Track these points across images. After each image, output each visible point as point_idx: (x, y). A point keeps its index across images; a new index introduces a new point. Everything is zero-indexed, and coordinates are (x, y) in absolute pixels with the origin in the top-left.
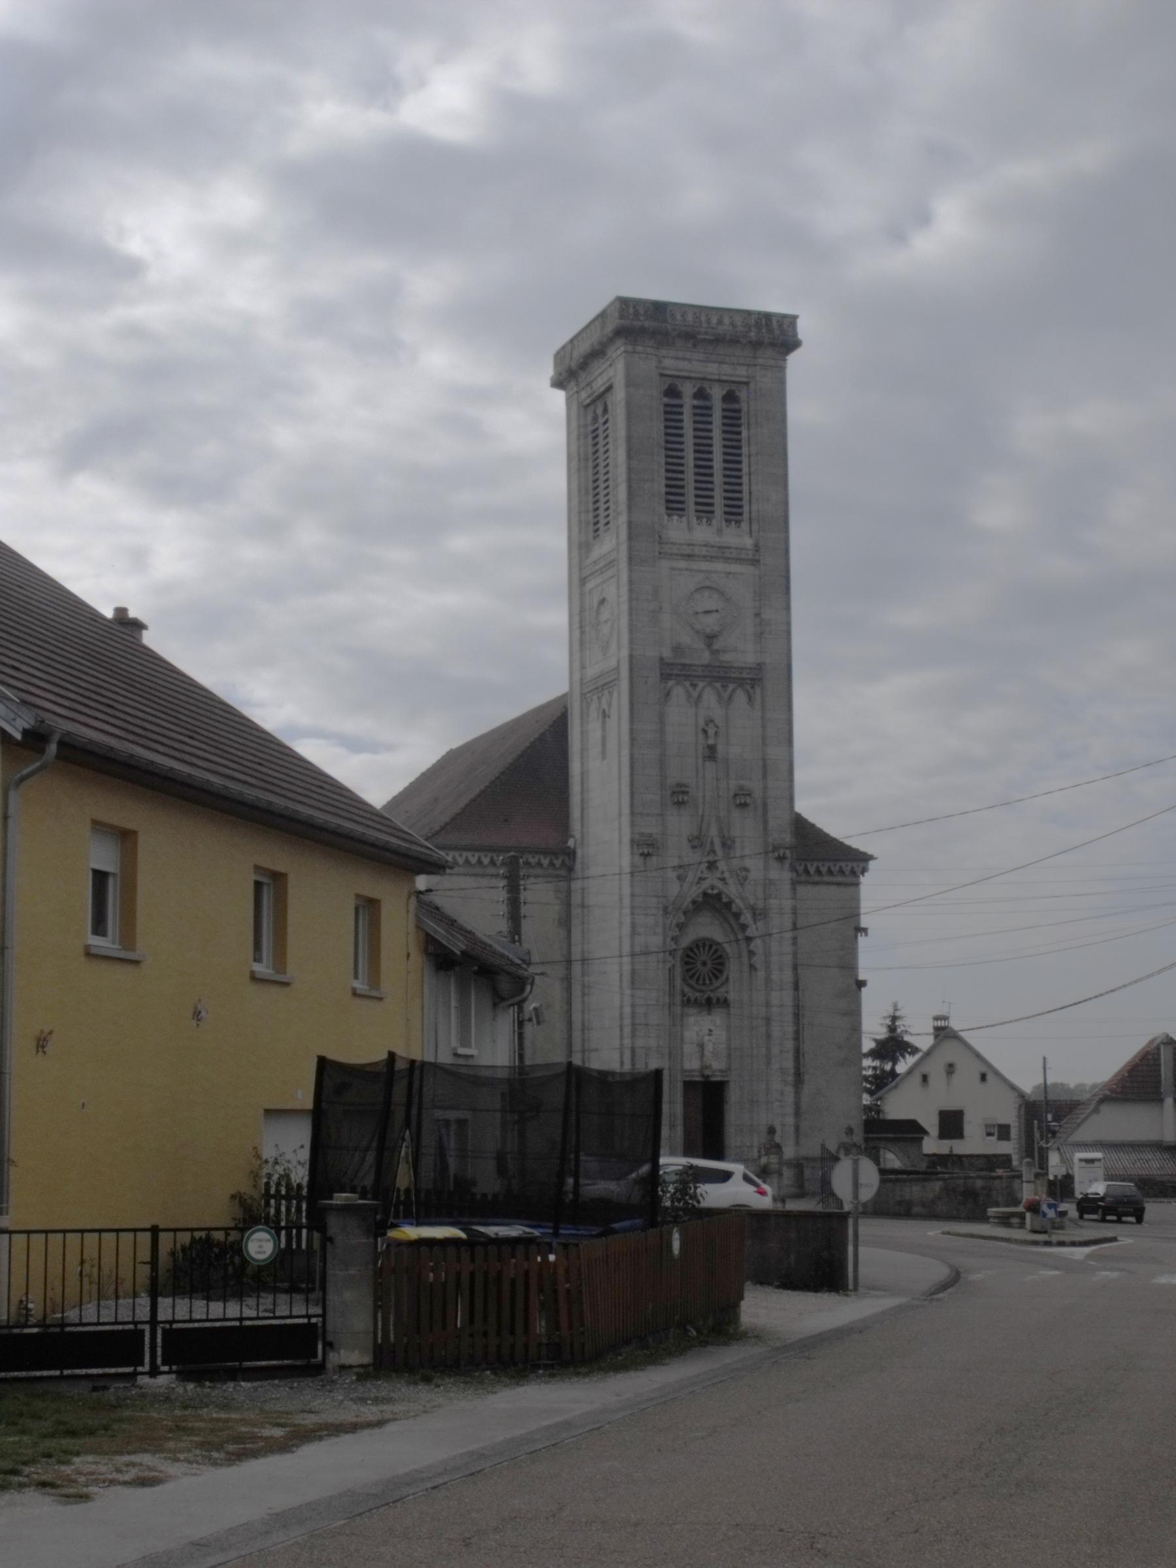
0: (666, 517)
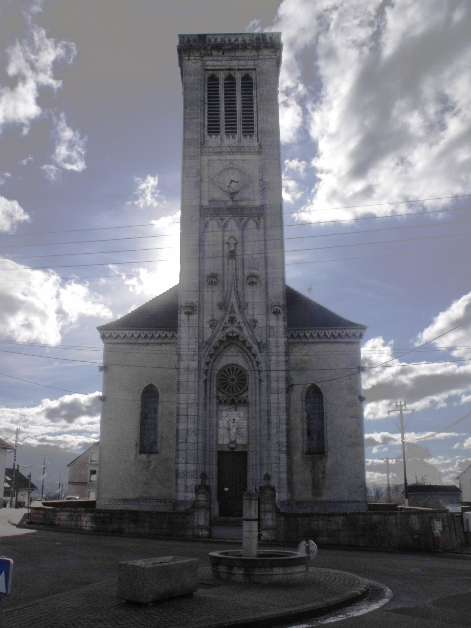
0: (208, 137)
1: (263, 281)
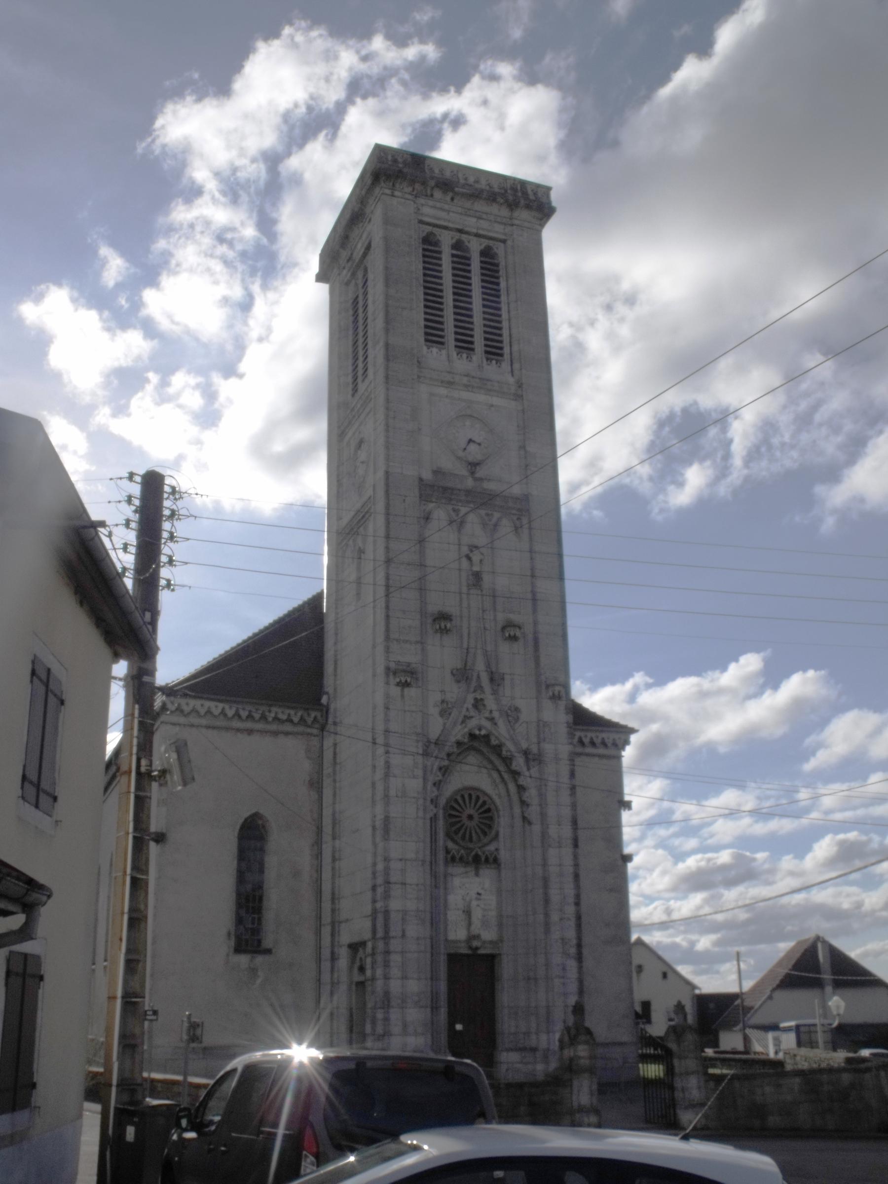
0: (425, 348)
1: (530, 637)
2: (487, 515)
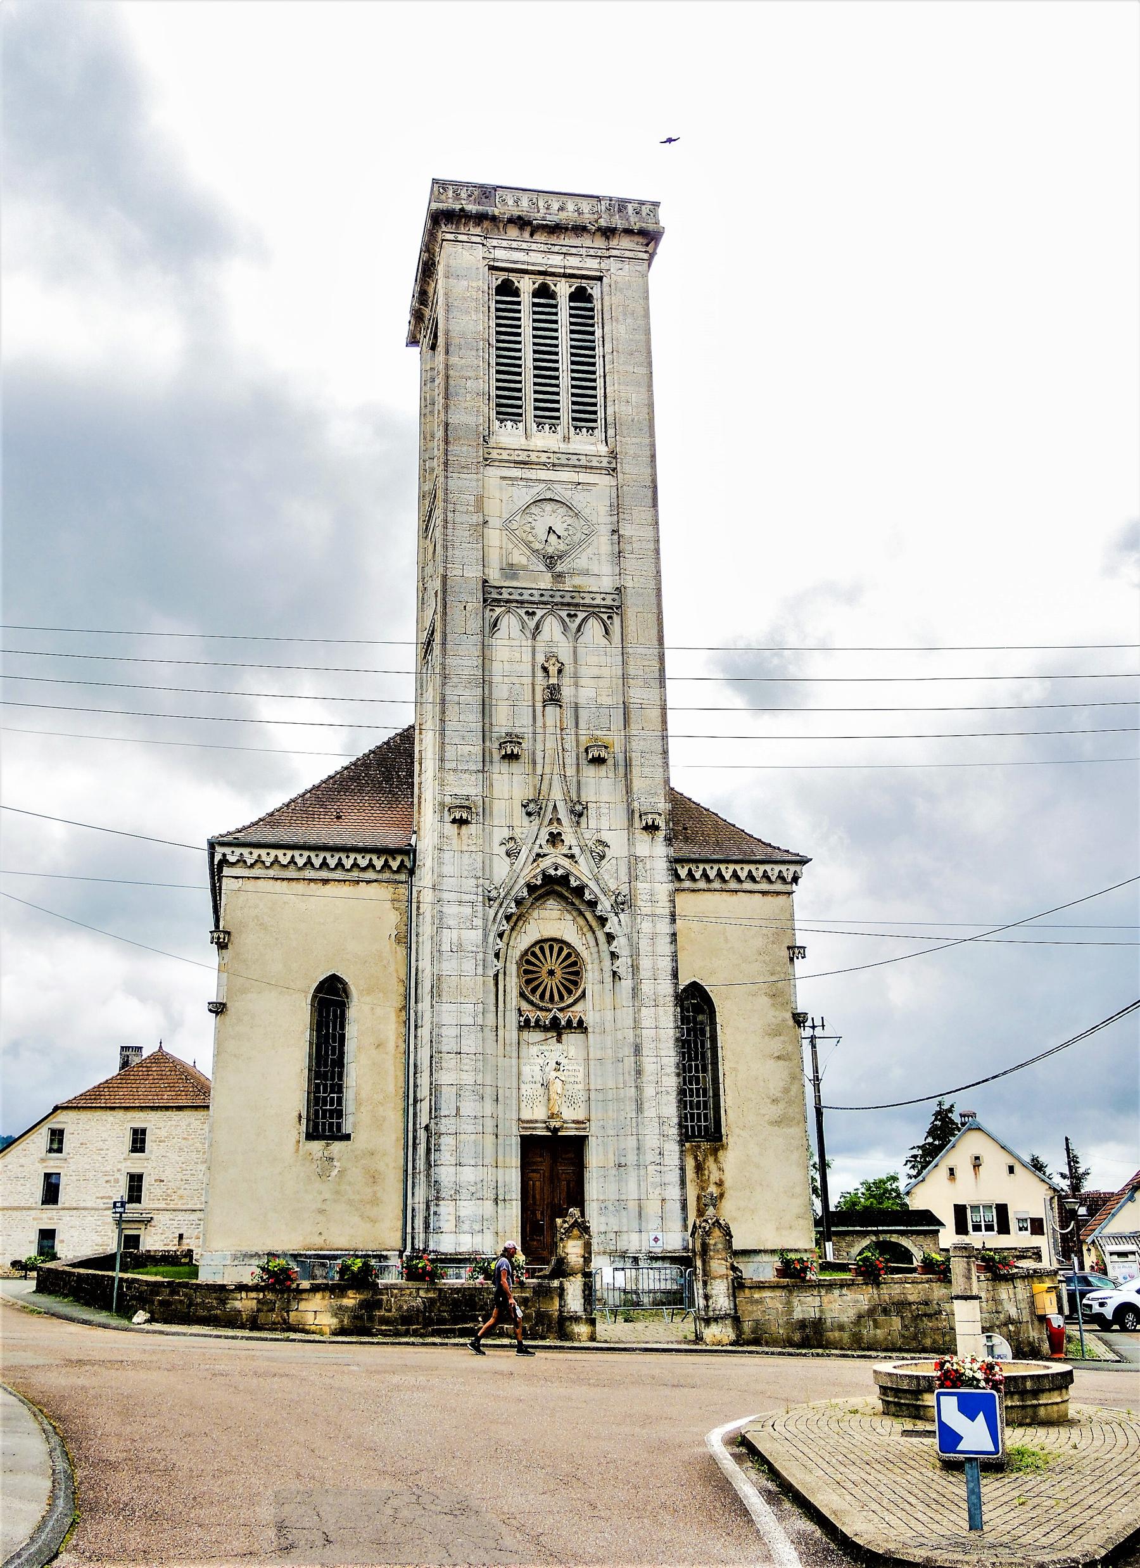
1: (621, 757)
2: (569, 615)
